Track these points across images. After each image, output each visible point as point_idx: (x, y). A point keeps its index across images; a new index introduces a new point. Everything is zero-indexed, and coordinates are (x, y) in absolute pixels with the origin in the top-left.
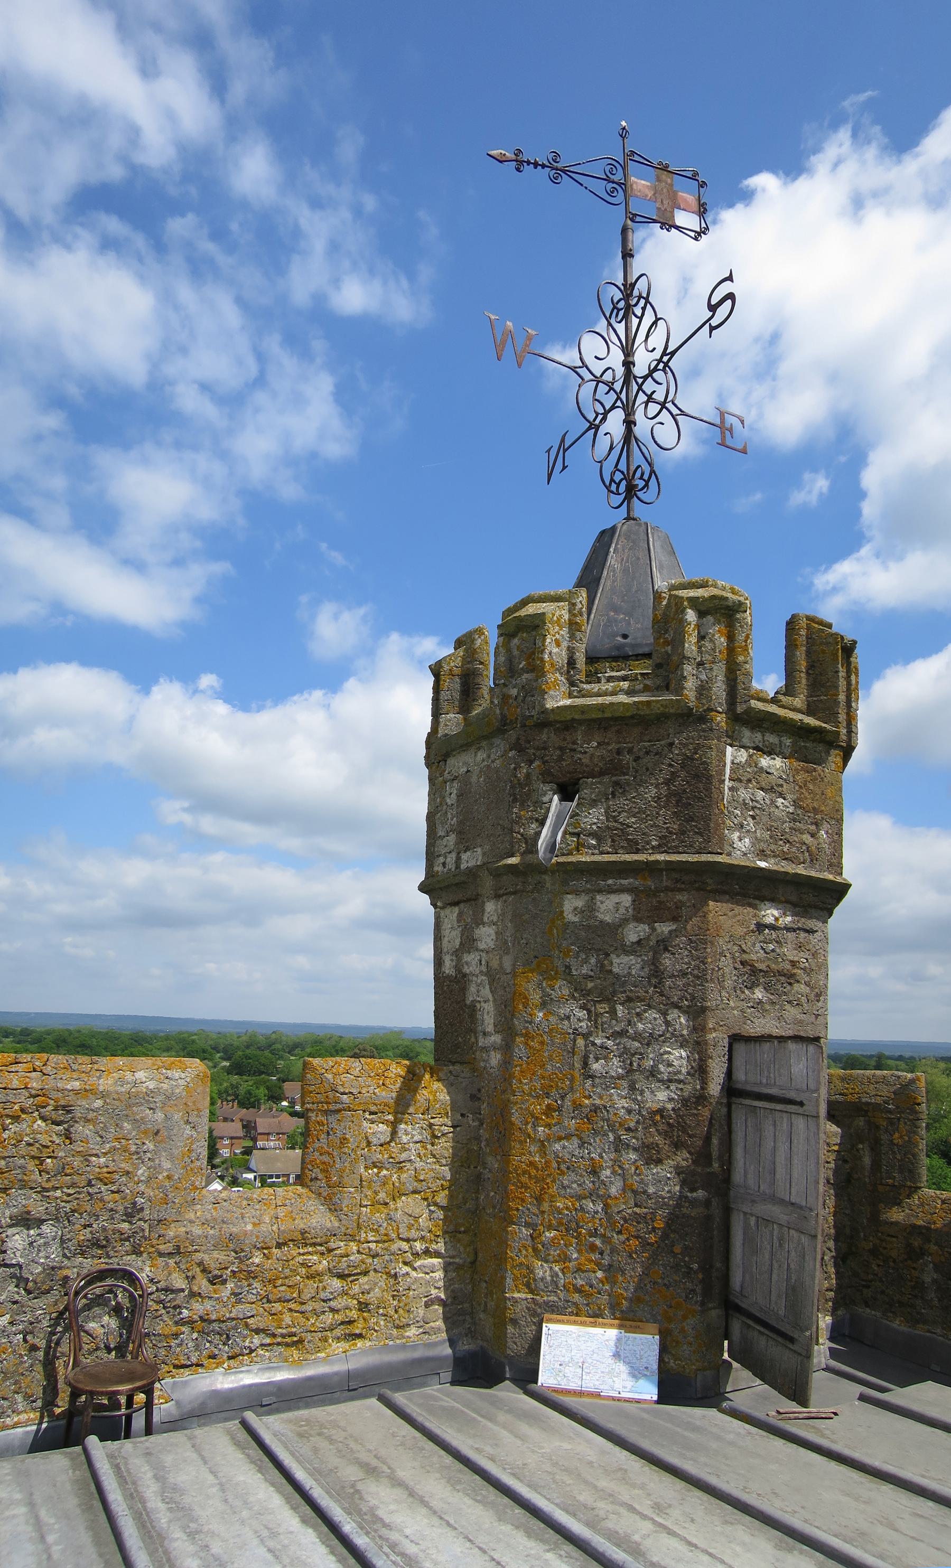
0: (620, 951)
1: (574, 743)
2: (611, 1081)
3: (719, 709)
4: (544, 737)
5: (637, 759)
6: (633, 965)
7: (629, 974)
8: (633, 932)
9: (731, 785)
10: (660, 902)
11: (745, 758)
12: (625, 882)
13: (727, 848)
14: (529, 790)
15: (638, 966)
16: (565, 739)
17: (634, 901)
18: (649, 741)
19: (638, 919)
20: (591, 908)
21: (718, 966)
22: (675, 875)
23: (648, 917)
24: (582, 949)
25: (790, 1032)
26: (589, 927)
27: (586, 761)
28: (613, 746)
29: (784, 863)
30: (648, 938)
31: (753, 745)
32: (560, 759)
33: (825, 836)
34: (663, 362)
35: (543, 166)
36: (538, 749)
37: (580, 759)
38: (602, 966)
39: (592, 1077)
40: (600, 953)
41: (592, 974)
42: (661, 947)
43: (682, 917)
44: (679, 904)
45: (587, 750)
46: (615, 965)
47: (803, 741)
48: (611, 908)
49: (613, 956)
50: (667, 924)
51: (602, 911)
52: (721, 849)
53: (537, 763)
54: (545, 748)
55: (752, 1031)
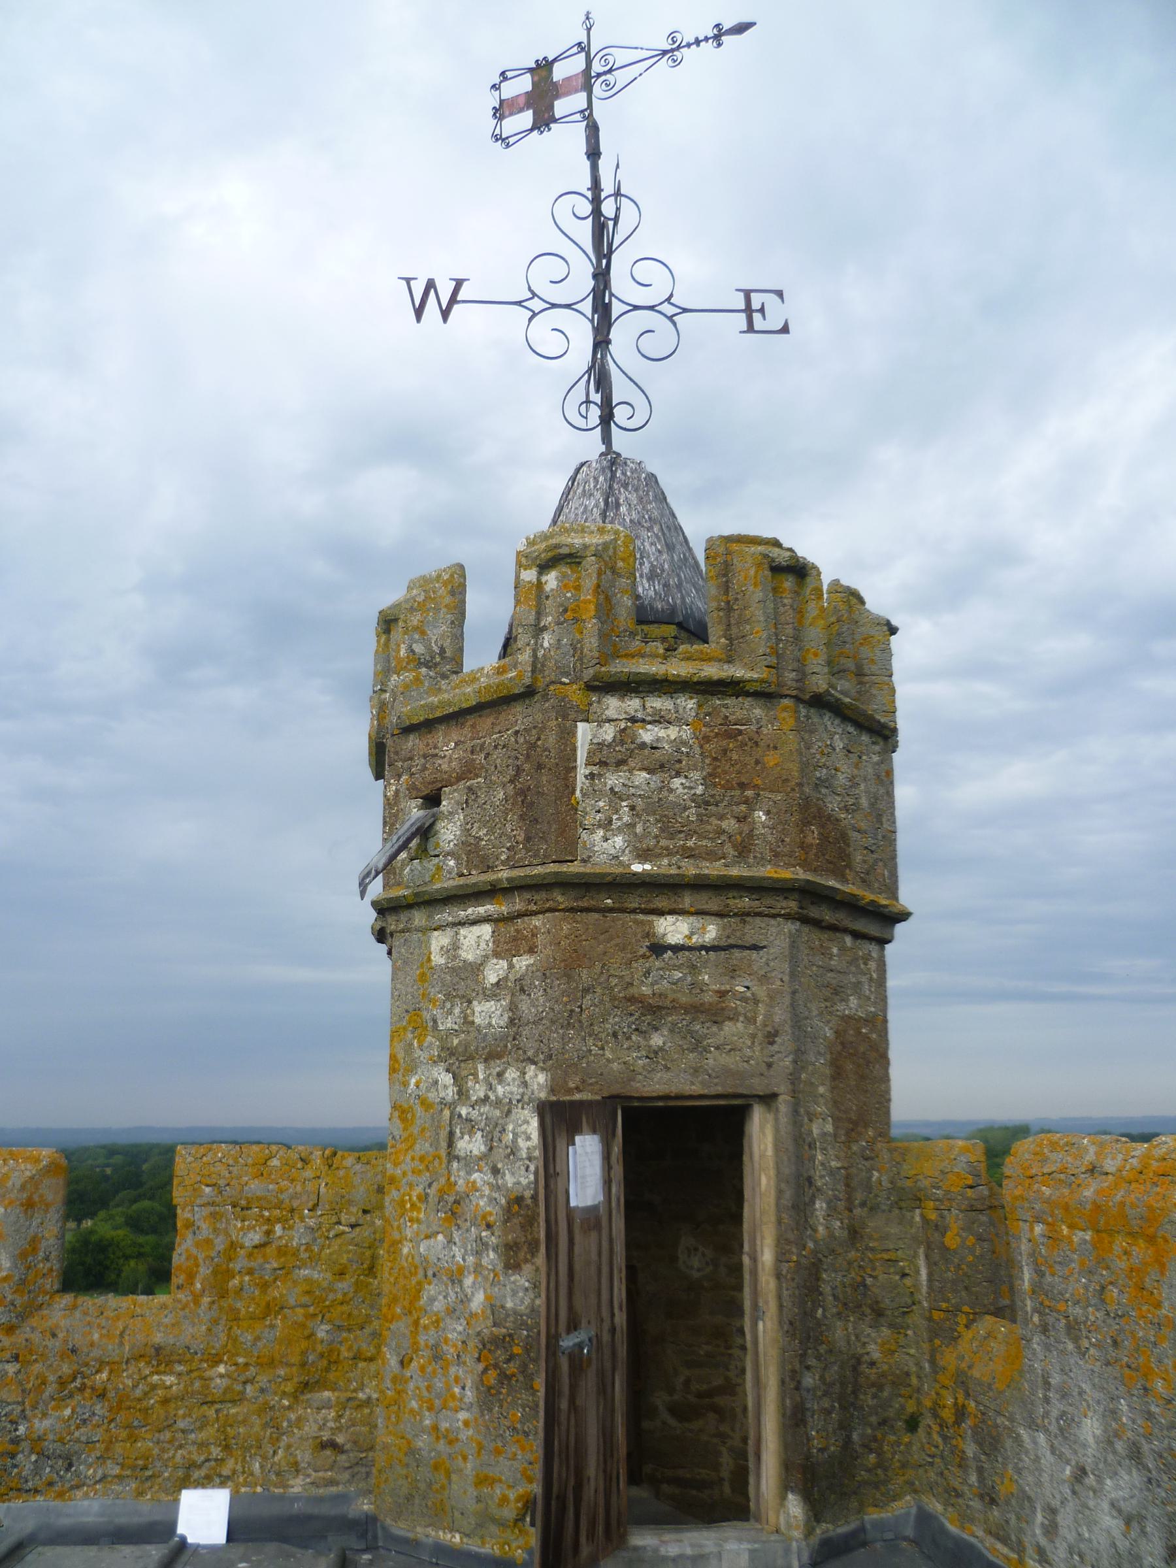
0: (481, 996)
1: (435, 747)
2: (470, 1163)
3: (564, 680)
4: (410, 744)
5: (487, 755)
6: (493, 1012)
7: (490, 1024)
8: (493, 973)
9: (587, 772)
10: (517, 931)
11: (612, 735)
12: (481, 910)
13: (581, 854)
14: (398, 810)
15: (498, 1012)
16: (428, 745)
17: (493, 932)
18: (499, 732)
19: (497, 954)
20: (456, 946)
21: (580, 1007)
22: (527, 895)
23: (507, 950)
24: (448, 997)
25: (720, 1088)
26: (453, 969)
27: (445, 767)
28: (469, 745)
29: (685, 863)
30: (506, 978)
31: (624, 716)
32: (424, 769)
33: (764, 818)
34: (605, 255)
35: (689, 45)
36: (404, 761)
37: (440, 765)
38: (465, 1017)
39: (458, 1158)
40: (464, 1000)
41: (456, 1027)
42: (518, 988)
43: (537, 947)
44: (535, 931)
45: (447, 753)
46: (477, 1014)
47: (719, 699)
48: (473, 943)
49: (475, 1003)
50: (524, 957)
51: (465, 948)
52: (571, 854)
53: (404, 777)
54: (411, 759)
55: (646, 1089)
